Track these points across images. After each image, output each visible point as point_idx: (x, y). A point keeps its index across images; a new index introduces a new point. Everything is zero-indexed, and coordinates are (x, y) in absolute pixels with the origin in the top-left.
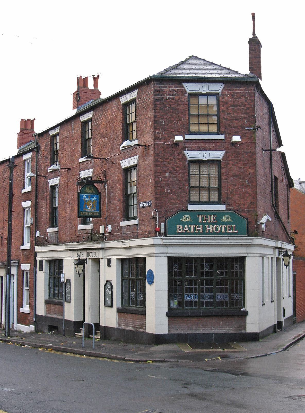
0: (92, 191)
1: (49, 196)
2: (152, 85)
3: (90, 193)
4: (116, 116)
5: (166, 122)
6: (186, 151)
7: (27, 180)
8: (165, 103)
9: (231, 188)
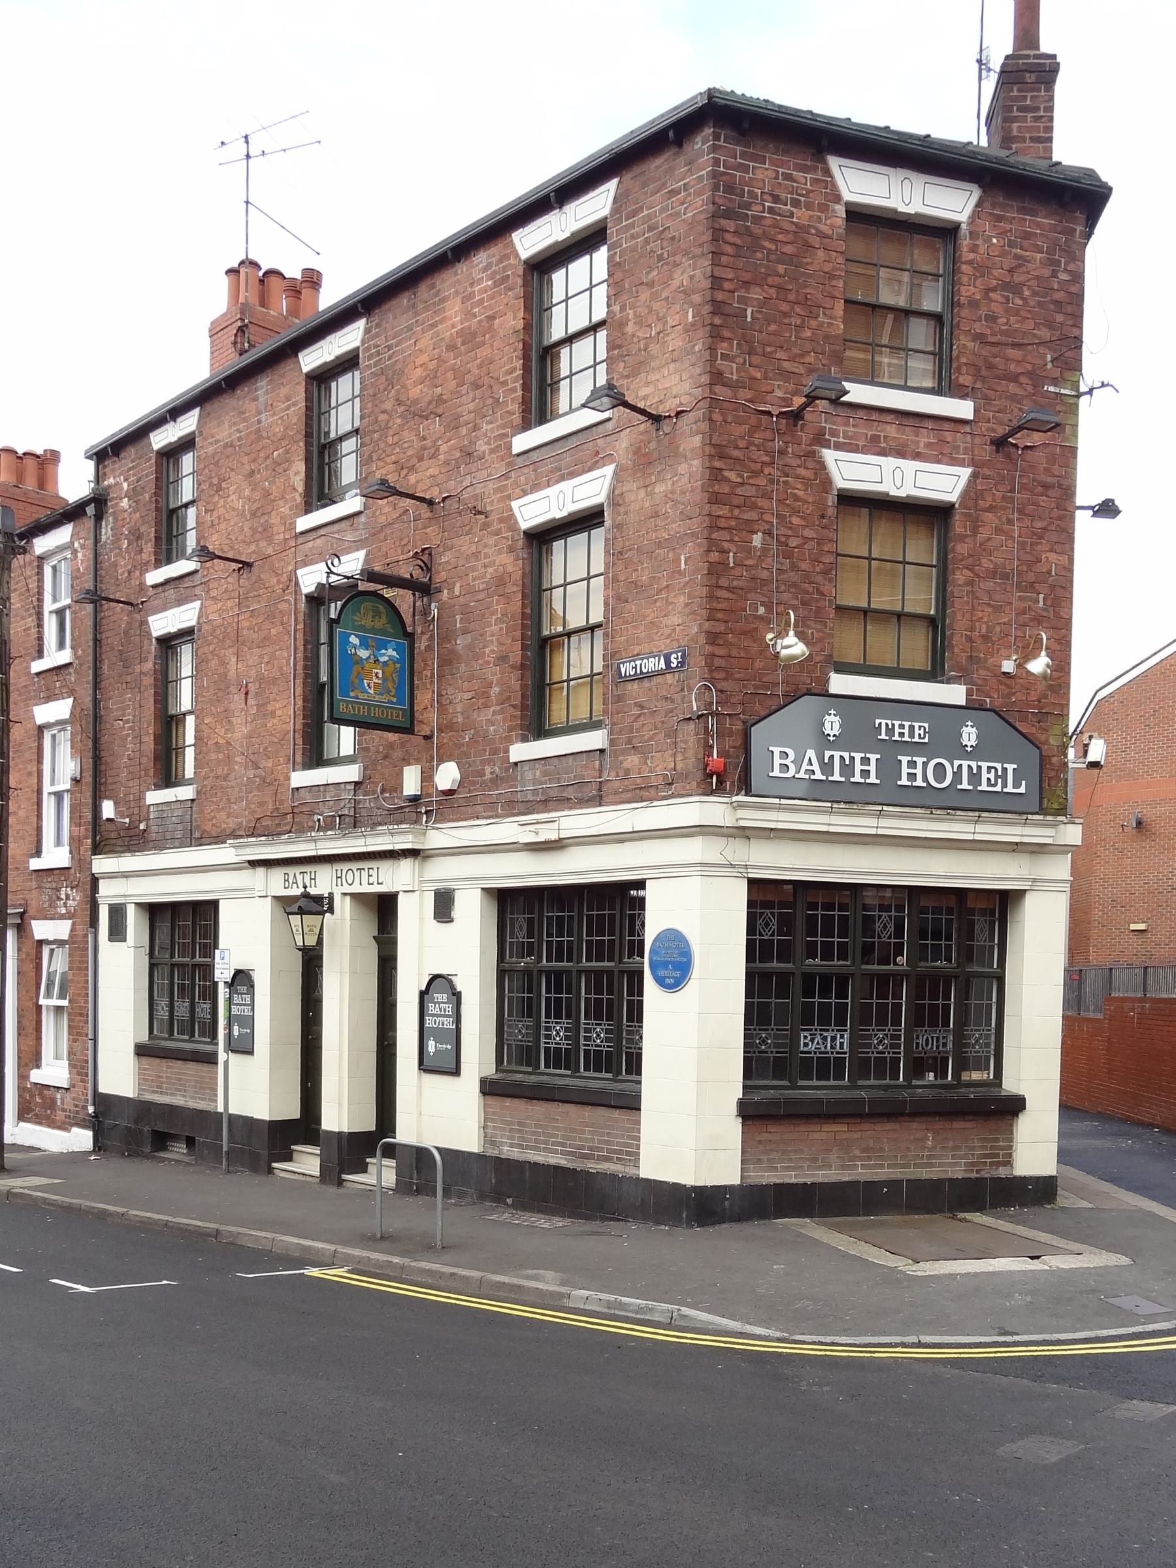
0: (382, 622)
1: (152, 672)
2: (701, 143)
3: (373, 630)
4: (491, 318)
5: (759, 316)
6: (829, 448)
7: (50, 626)
8: (757, 230)
9: (985, 619)
